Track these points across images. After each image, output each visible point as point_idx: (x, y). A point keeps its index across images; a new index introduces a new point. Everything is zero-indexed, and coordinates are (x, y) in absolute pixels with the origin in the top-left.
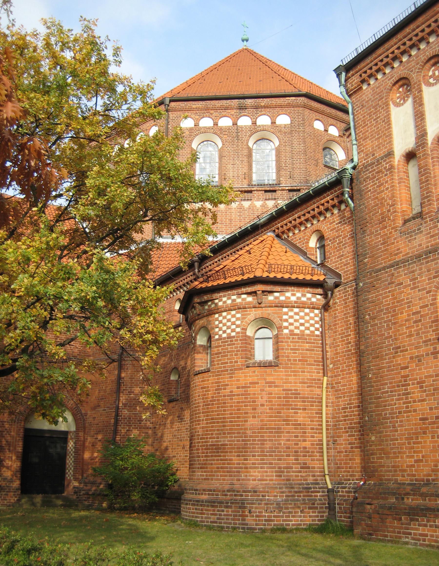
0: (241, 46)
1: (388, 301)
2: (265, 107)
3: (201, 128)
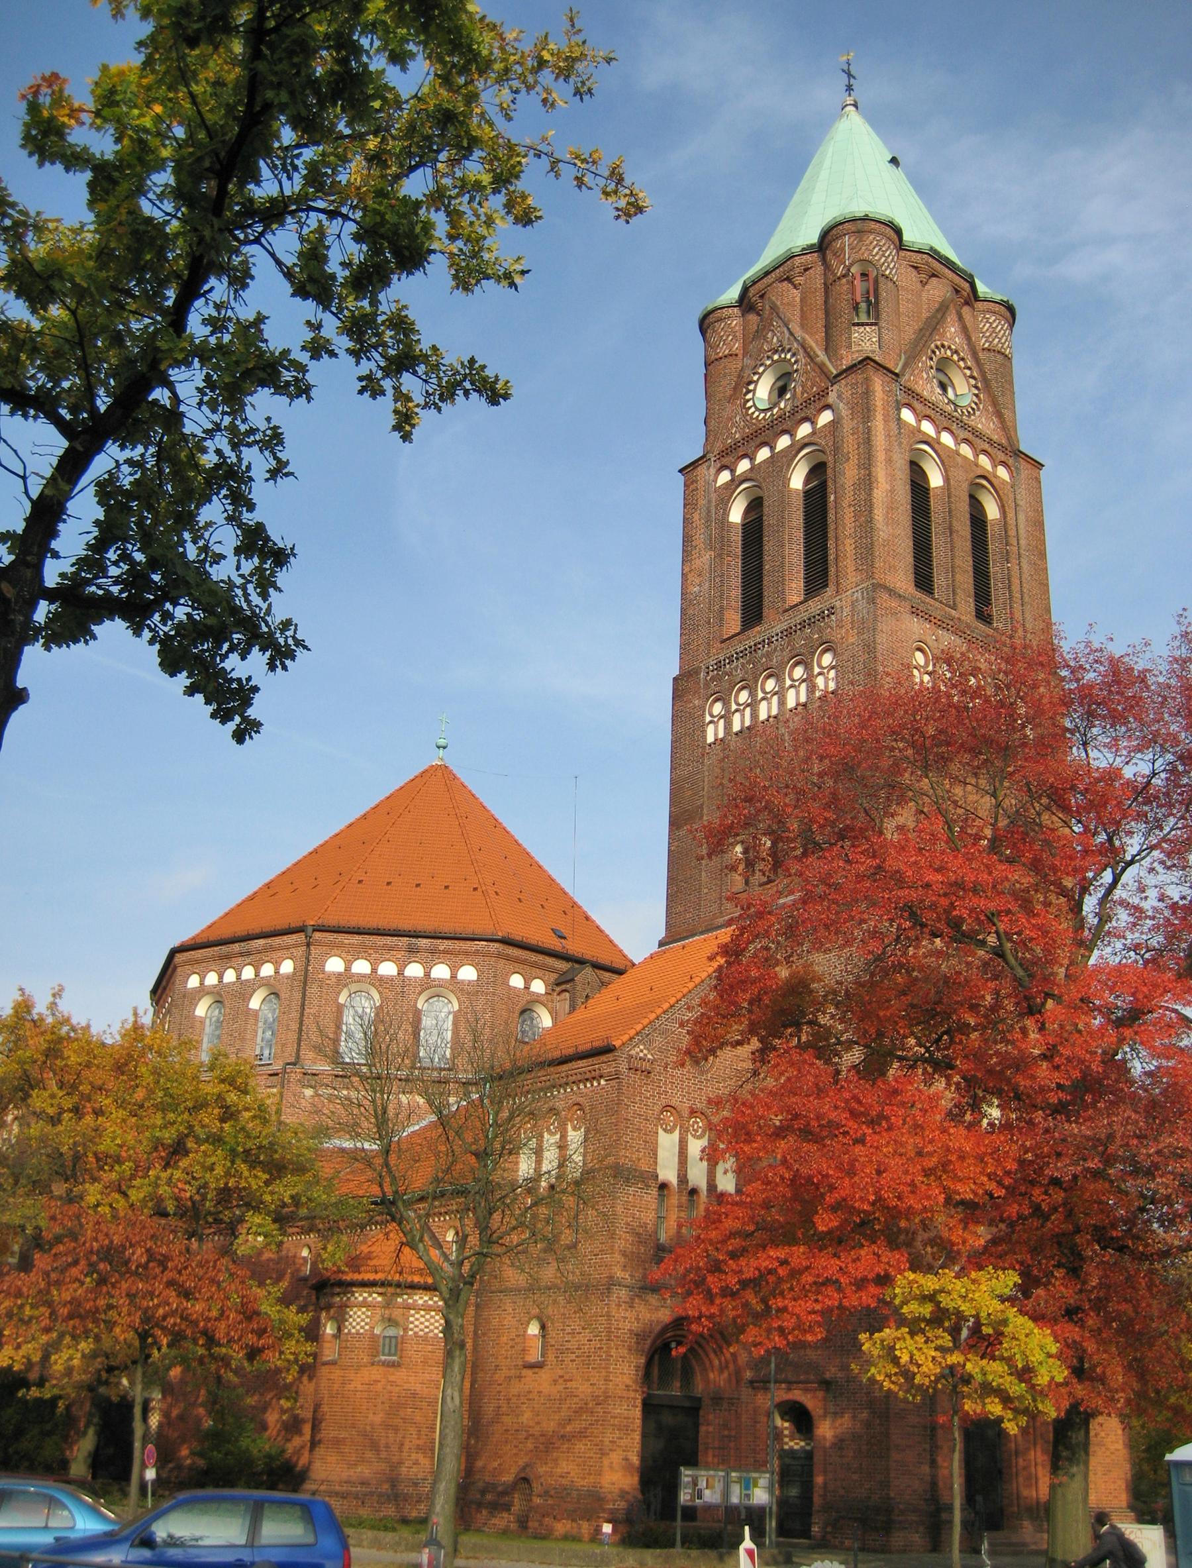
0: (435, 759)
1: (495, 1322)
2: (445, 952)
3: (353, 975)
